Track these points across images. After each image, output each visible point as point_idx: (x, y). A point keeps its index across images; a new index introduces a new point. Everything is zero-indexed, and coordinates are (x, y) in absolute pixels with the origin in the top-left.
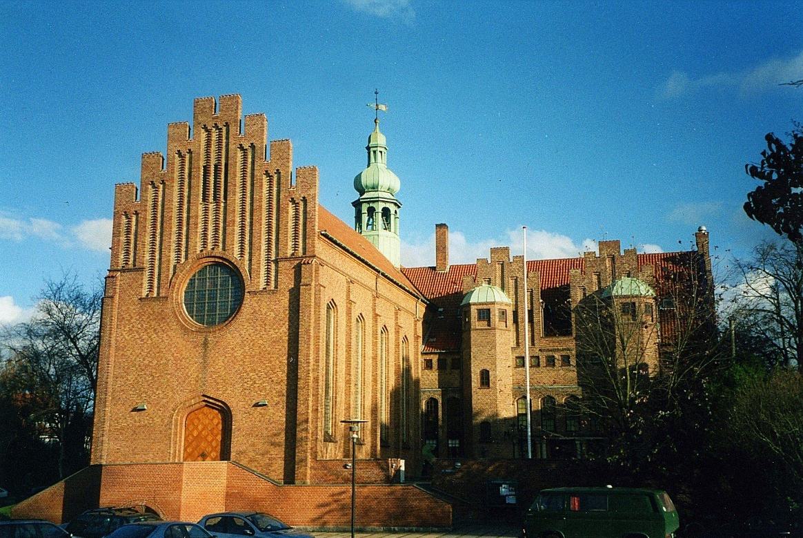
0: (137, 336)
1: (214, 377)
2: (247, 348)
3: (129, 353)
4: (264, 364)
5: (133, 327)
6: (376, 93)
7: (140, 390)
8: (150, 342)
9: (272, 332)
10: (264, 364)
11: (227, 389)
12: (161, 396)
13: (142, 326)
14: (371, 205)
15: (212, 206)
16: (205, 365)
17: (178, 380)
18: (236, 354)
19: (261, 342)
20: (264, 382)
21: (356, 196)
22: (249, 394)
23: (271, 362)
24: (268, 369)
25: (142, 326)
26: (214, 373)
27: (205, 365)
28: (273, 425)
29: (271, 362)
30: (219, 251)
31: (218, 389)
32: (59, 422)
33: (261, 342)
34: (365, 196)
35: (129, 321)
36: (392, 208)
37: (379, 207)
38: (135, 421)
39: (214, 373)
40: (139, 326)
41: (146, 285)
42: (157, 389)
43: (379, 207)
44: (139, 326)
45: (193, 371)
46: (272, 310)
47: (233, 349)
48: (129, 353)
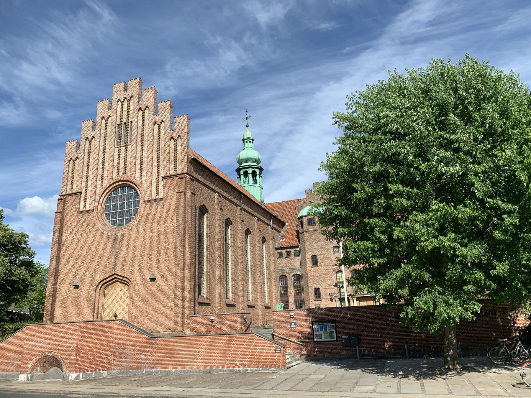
0: (75, 237)
1: (121, 260)
2: (142, 239)
3: (70, 248)
4: (154, 250)
5: (73, 230)
6: (247, 111)
7: (75, 273)
8: (82, 240)
9: (159, 227)
10: (154, 250)
11: (129, 269)
12: (88, 276)
13: (78, 230)
14: (245, 170)
15: (123, 149)
16: (115, 253)
17: (98, 265)
18: (135, 244)
19: (151, 234)
20: (153, 262)
21: (238, 165)
22: (144, 271)
23: (158, 248)
24: (156, 253)
25: (78, 230)
26: (121, 258)
27: (115, 253)
28: (159, 292)
29: (158, 248)
30: (122, 176)
31: (124, 269)
32: (477, 207)
33: (151, 234)
34: (243, 165)
35: (70, 227)
36: (258, 171)
37: (250, 171)
38: (72, 294)
39: (121, 258)
40: (76, 230)
41: (82, 204)
42: (86, 271)
43: (250, 171)
44: (76, 230)
45: (108, 258)
46: (159, 212)
47: (133, 241)
48: (70, 248)
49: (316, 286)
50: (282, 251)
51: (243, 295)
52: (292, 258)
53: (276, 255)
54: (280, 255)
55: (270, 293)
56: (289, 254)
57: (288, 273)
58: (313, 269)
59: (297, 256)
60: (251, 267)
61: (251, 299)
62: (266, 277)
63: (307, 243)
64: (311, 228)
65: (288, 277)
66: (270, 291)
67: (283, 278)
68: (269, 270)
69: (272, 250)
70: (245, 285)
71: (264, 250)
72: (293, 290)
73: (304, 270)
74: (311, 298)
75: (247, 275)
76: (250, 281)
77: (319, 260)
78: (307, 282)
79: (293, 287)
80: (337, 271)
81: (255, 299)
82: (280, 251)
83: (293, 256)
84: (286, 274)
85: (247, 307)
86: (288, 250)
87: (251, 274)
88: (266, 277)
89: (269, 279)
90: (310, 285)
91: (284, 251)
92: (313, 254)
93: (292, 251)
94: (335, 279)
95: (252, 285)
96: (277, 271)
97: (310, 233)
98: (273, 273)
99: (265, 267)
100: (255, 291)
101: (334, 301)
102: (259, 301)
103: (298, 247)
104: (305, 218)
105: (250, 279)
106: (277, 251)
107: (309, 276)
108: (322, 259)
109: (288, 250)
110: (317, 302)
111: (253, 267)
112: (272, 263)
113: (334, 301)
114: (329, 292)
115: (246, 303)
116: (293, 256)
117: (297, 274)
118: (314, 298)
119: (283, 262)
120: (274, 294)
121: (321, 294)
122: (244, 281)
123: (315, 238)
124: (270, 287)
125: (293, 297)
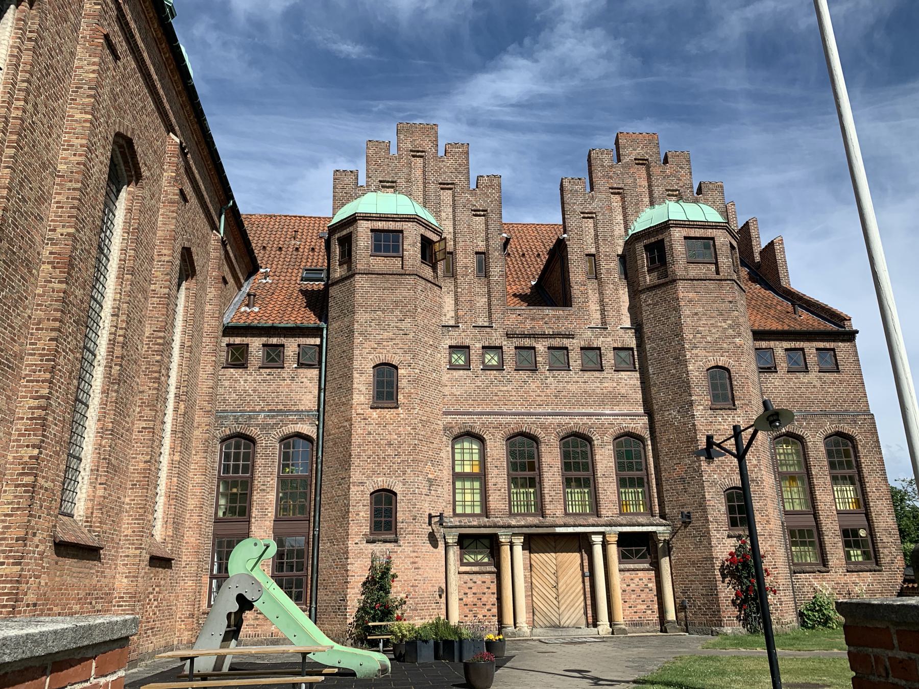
49: (381, 482)
50: (246, 340)
51: (33, 468)
52: (285, 373)
53: (223, 356)
54: (238, 358)
55: (177, 497)
56: (274, 357)
57: (264, 427)
58: (375, 414)
59: (310, 366)
60: (112, 343)
61: (80, 509)
62: (168, 427)
63: (361, 317)
64: (380, 263)
65: (262, 442)
66: (177, 496)
67: (239, 447)
68: (185, 395)
69: (211, 325)
70: (59, 404)
71: (180, 309)
72: (272, 497)
73: (332, 420)
74: (353, 529)
75: (82, 376)
76: (93, 413)
77: (403, 383)
78: (345, 463)
79: (274, 482)
80: (456, 431)
81: (107, 509)
82: (238, 340)
83: (291, 363)
84: (254, 432)
85: (47, 548)
86: (274, 341)
87: (108, 375)
88: (168, 427)
89: (183, 435)
90: (356, 475)
91: (256, 344)
92: (383, 358)
93: (291, 346)
94: (448, 463)
95: (102, 432)
96: (220, 417)
97: (379, 281)
98: (199, 418)
99: (173, 381)
100: (111, 467)
101: (441, 545)
102: (127, 525)
103: (316, 332)
104: (364, 227)
105: (95, 402)
106: (226, 340)
107: (356, 439)
108: (415, 381)
109: (274, 341)
110: (378, 548)
111: (123, 344)
112: (202, 375)
113: (441, 545)
114: (427, 508)
115: (43, 523)
116: (291, 363)
117: (299, 435)
118: (366, 530)
119: (247, 383)
120: (192, 503)
121: (400, 516)
122: (61, 380)
123: (396, 303)
124: (180, 469)
125: (269, 523)
